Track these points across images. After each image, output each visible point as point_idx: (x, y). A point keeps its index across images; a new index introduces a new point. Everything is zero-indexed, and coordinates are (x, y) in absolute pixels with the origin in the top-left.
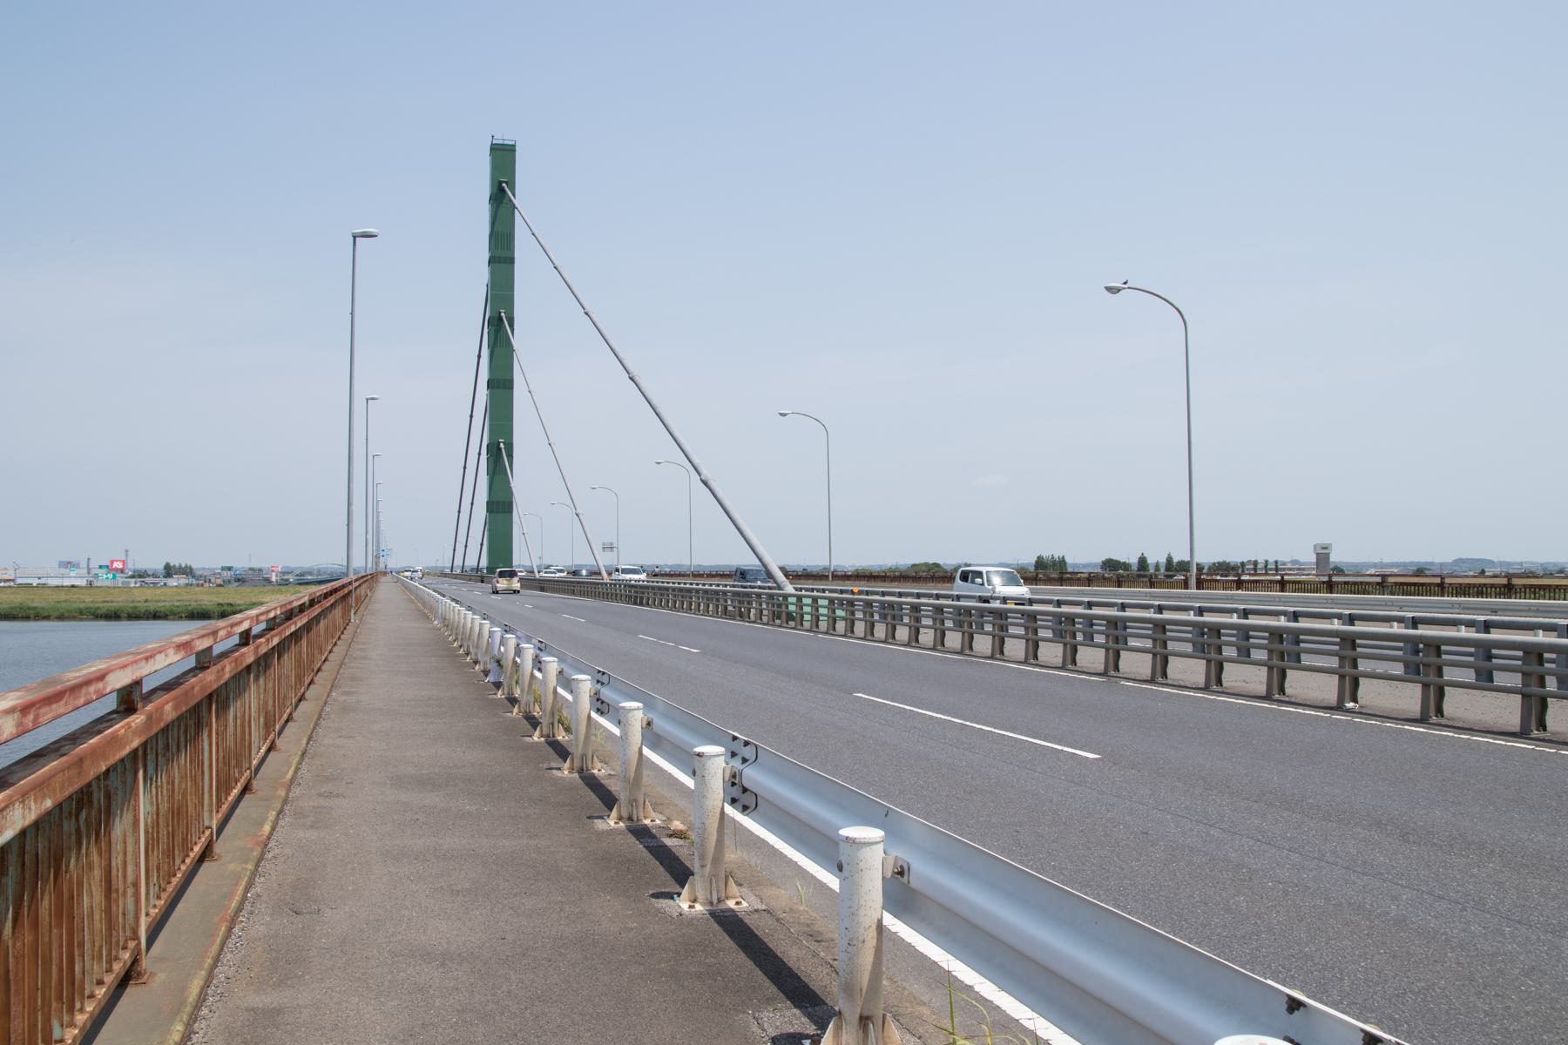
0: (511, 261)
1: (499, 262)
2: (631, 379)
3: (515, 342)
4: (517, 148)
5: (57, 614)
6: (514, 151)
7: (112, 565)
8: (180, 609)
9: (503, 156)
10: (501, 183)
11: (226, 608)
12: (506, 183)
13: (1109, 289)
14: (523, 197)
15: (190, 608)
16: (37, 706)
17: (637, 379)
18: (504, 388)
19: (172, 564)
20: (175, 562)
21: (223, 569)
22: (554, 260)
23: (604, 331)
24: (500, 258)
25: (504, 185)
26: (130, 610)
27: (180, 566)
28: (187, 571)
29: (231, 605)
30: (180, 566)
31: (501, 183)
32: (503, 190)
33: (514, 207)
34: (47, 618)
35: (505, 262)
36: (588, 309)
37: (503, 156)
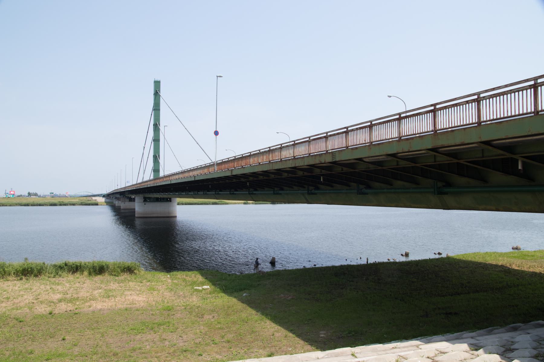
0: (159, 110)
1: (156, 110)
2: (197, 143)
3: (160, 128)
4: (161, 82)
5: (9, 205)
6: (160, 82)
7: (10, 193)
8: (47, 203)
9: (157, 84)
10: (157, 90)
11: (61, 203)
12: (158, 90)
13: (277, 133)
14: (162, 93)
15: (50, 203)
16: (84, 203)
17: (198, 143)
18: (158, 141)
19: (31, 192)
20: (31, 192)
21: (50, 193)
22: (176, 115)
23: (190, 133)
24: (156, 109)
25: (158, 91)
26: (32, 204)
27: (33, 193)
28: (36, 195)
29: (63, 202)
30: (33, 193)
31: (157, 90)
32: (157, 92)
33: (160, 96)
34: (6, 206)
35: (158, 110)
36: (186, 127)
37: (157, 84)
